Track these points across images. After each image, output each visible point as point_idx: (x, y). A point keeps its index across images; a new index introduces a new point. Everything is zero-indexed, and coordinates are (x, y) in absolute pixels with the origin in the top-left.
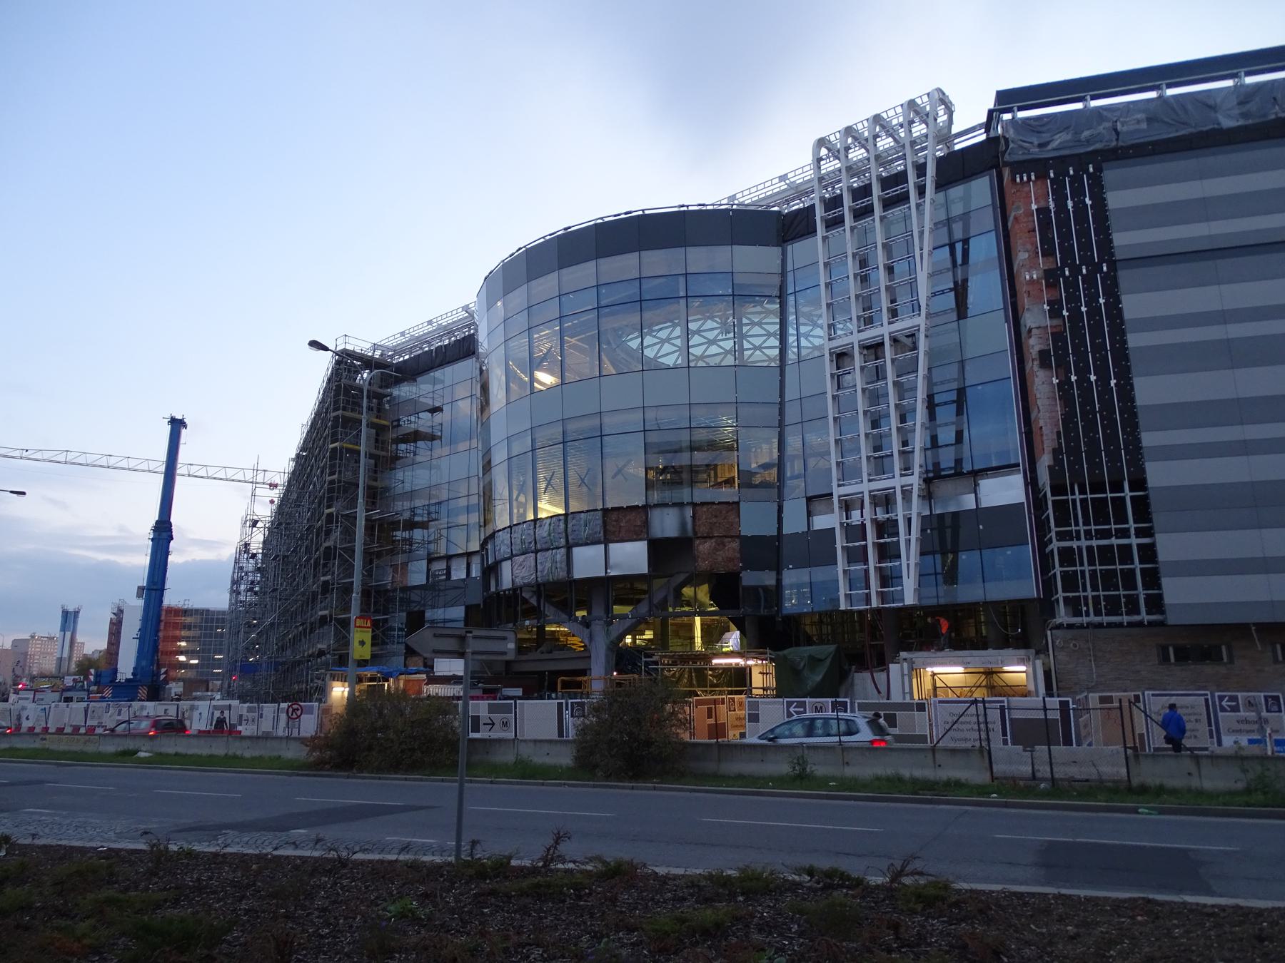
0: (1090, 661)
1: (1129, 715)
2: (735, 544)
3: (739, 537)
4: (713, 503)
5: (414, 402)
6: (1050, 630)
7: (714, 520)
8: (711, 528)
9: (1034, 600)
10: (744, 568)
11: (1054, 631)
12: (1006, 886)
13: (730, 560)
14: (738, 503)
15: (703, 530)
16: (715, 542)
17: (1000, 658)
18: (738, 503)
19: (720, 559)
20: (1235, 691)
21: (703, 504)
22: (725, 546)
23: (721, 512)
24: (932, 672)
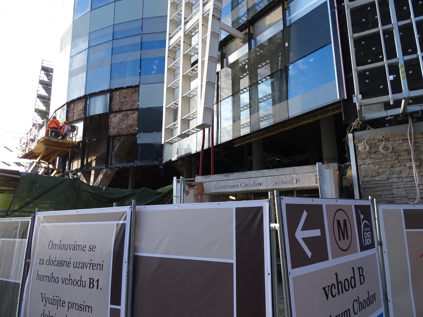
0: (411, 168)
1: (125, 39)
2: (135, 115)
3: (137, 109)
4: (122, 88)
5: (216, 144)
6: (353, 132)
7: (124, 100)
8: (121, 106)
9: (339, 102)
10: (139, 131)
11: (356, 133)
12: (382, 300)
13: (131, 126)
14: (138, 86)
15: (116, 107)
16: (122, 115)
17: (295, 176)
18: (138, 86)
19: (124, 126)
20: (371, 235)
21: (117, 89)
22: (128, 117)
23: (128, 94)
24: (33, 161)
